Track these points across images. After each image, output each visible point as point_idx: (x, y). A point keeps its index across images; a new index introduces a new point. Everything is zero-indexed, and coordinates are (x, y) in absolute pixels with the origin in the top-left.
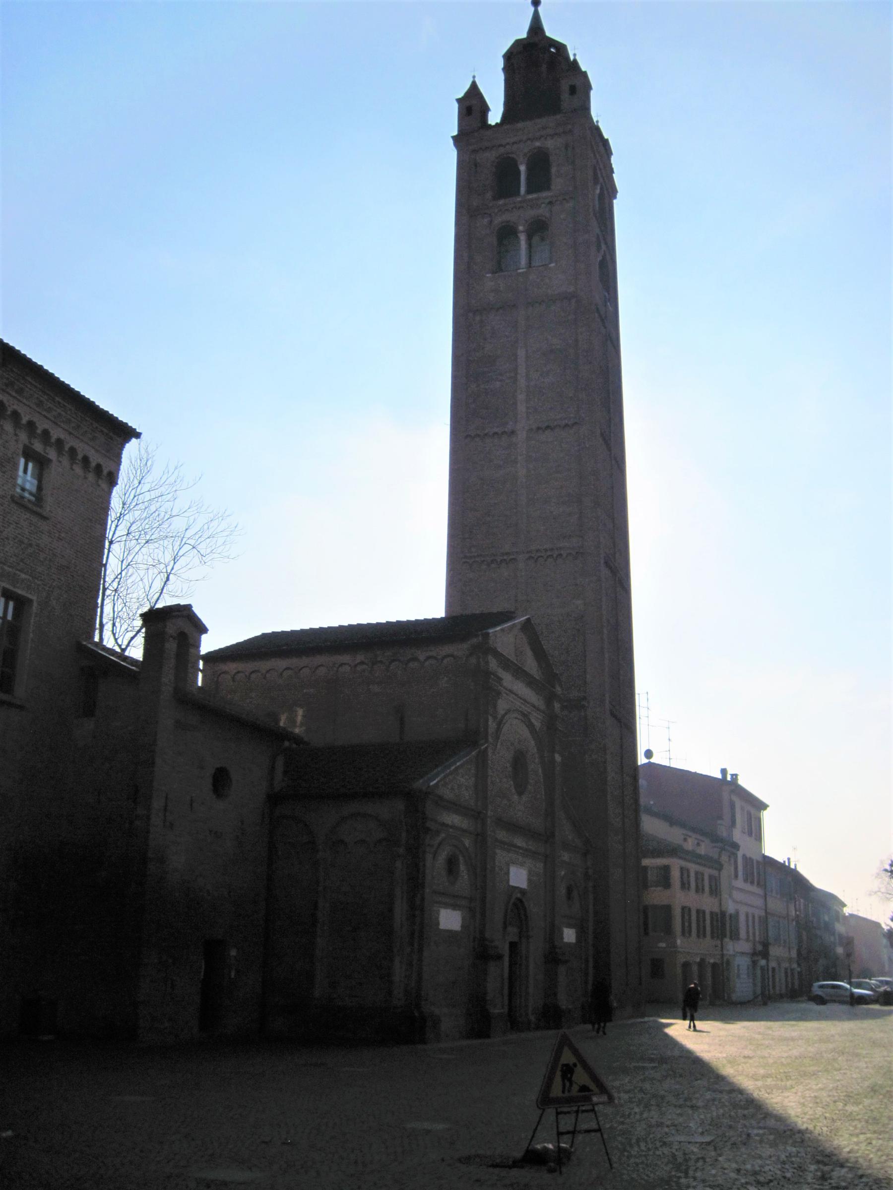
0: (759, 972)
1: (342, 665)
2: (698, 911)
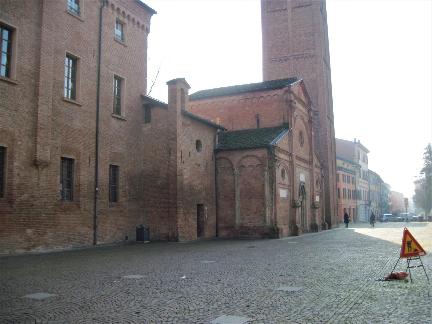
0: (367, 211)
1: (234, 100)
2: (348, 190)
